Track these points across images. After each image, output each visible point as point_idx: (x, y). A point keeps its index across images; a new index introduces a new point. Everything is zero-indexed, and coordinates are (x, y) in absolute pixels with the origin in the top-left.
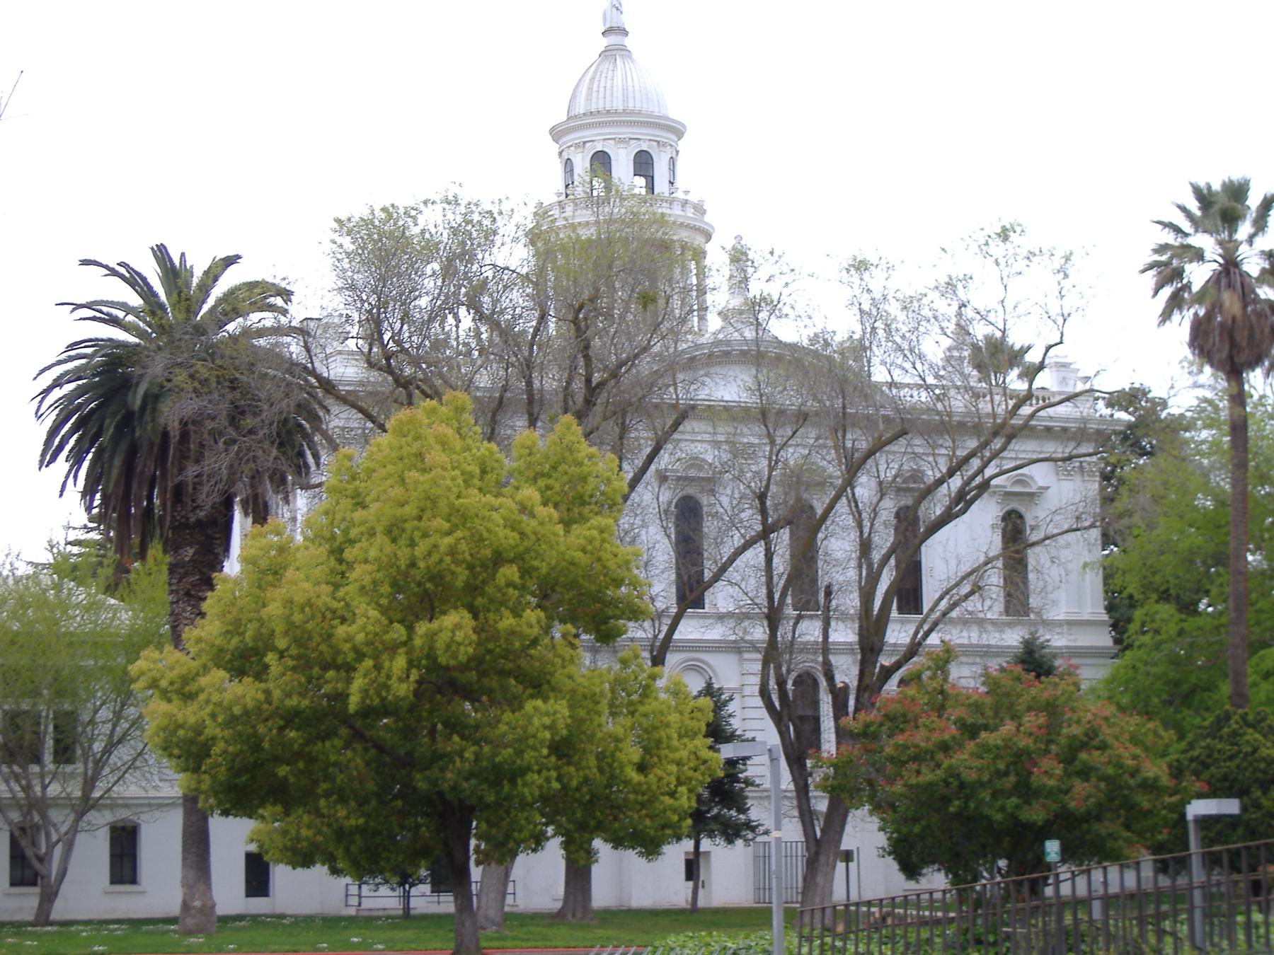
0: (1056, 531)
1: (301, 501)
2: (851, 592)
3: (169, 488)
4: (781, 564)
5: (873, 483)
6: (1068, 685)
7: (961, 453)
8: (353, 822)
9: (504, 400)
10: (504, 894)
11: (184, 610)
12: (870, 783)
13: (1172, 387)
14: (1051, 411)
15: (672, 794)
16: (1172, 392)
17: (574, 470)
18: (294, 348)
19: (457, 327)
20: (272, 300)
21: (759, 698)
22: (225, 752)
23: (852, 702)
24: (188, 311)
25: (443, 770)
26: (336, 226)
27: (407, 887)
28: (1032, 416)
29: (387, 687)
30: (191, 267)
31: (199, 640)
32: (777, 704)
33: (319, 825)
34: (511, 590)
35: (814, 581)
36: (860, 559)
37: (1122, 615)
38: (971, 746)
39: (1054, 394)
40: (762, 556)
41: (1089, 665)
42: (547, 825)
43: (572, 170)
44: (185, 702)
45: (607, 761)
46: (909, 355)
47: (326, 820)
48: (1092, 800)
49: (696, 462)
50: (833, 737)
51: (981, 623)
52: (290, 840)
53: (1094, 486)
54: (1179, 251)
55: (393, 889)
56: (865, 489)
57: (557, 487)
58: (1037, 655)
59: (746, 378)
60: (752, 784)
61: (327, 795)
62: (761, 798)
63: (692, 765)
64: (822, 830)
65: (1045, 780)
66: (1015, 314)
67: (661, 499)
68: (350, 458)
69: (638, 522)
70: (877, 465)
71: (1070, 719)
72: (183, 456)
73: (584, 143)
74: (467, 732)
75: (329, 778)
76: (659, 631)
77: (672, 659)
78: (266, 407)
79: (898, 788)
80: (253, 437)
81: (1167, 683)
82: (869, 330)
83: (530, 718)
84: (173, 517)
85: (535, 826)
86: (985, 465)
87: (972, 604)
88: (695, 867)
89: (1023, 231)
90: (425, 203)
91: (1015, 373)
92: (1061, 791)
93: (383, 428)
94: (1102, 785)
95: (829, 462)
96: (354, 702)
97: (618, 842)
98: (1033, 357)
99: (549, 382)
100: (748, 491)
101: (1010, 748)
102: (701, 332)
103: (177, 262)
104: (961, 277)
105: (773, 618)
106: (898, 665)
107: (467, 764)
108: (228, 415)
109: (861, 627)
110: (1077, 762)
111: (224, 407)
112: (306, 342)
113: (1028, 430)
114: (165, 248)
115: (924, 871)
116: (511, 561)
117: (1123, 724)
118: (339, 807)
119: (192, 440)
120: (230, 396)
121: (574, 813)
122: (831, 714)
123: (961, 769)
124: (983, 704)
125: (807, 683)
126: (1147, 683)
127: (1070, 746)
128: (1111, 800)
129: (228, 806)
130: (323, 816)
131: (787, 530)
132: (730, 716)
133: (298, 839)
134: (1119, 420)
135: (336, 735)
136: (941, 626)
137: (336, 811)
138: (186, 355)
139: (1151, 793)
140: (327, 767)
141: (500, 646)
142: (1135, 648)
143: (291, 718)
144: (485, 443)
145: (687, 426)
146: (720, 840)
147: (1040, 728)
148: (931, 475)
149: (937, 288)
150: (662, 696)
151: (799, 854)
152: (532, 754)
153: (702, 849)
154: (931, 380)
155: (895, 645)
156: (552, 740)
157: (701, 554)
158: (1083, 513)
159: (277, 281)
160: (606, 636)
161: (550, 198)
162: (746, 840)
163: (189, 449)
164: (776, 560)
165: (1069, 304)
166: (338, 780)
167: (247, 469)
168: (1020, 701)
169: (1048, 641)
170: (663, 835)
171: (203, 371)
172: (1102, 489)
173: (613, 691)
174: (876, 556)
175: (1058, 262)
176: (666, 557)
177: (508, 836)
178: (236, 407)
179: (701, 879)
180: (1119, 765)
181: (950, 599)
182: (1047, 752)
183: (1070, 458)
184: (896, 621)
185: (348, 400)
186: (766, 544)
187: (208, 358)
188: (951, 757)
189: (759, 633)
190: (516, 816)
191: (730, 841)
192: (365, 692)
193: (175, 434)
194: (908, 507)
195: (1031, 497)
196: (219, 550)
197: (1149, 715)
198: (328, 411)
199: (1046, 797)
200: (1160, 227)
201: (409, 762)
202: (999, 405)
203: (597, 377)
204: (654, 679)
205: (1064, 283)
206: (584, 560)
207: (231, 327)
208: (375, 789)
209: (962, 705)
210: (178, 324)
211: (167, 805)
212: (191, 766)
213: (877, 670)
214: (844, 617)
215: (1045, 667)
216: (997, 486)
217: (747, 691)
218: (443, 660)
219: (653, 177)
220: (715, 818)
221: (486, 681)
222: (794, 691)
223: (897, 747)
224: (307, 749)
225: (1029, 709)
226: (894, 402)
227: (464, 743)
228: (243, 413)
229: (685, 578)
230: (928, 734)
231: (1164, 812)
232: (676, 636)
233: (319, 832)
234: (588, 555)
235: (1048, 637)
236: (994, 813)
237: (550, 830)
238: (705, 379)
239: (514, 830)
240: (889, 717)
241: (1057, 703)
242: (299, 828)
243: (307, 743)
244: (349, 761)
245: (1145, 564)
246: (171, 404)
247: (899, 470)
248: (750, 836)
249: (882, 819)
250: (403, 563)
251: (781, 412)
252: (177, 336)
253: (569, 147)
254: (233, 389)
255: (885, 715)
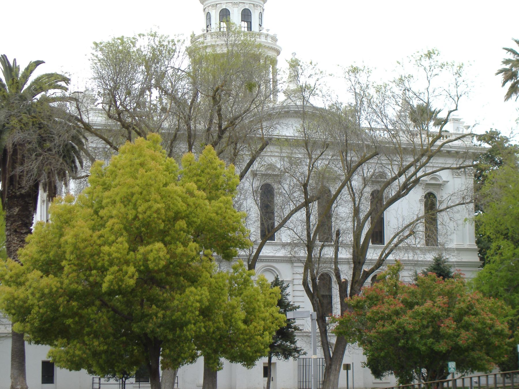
0: (452, 204)
1: (73, 185)
2: (349, 234)
3: (7, 178)
4: (314, 220)
5: (360, 179)
6: (430, 276)
7: (406, 164)
8: (102, 348)
9: (177, 136)
10: (173, 384)
11: (13, 239)
12: (359, 331)
13: (512, 133)
14: (450, 144)
15: (261, 335)
16: (512, 135)
17: (213, 172)
18: (71, 108)
19: (151, 96)
20: (59, 83)
21: (303, 286)
22: (39, 312)
23: (349, 289)
24: (17, 88)
25: (147, 322)
26: (94, 46)
27: (124, 379)
28: (442, 146)
29: (122, 281)
30: (19, 66)
31: (26, 255)
32: (311, 289)
33: (84, 349)
34: (182, 232)
35: (330, 228)
36: (354, 217)
37: (484, 245)
38: (410, 313)
39: (451, 134)
40: (304, 216)
41: (468, 271)
42: (197, 350)
43: (210, 18)
44: (18, 287)
45: (228, 318)
46: (380, 115)
47: (88, 347)
48: (470, 340)
49: (271, 167)
50: (339, 306)
51: (414, 249)
52: (70, 356)
53: (470, 181)
54: (516, 63)
55: (117, 380)
56: (356, 182)
57: (204, 180)
58: (442, 266)
59: (298, 126)
60: (298, 329)
61: (88, 334)
62: (303, 336)
63: (270, 320)
64: (333, 353)
65: (447, 330)
66: (434, 95)
67: (254, 186)
68: (101, 165)
69: (242, 197)
70: (363, 170)
71: (460, 300)
72: (14, 162)
73: (216, 4)
74: (159, 304)
75: (91, 326)
76: (252, 252)
77: (259, 266)
78: (57, 137)
79: (373, 333)
80: (50, 152)
81: (507, 280)
82: (359, 102)
83: (188, 297)
84: (8, 192)
85: (192, 351)
86: (417, 171)
87: (410, 241)
88: (269, 370)
89: (438, 53)
90: (140, 35)
91: (432, 123)
92: (455, 336)
93: (117, 149)
94: (476, 333)
95: (339, 169)
96: (105, 287)
97: (233, 359)
98: (442, 115)
99: (201, 126)
100: (298, 182)
101: (429, 314)
102: (275, 101)
103: (11, 64)
104: (407, 76)
105: (310, 246)
106: (372, 271)
107: (159, 320)
108: (38, 141)
109: (354, 251)
110: (463, 321)
111: (34, 138)
112: (77, 105)
113: (439, 152)
114: (6, 56)
115: (384, 374)
116: (182, 218)
117: (486, 303)
118: (95, 340)
119: (18, 153)
120: (38, 132)
121: (212, 345)
122: (339, 295)
123: (405, 324)
124: (416, 292)
125: (326, 278)
126: (497, 280)
127: (460, 313)
128: (480, 340)
129: (39, 339)
130: (86, 345)
131: (317, 202)
132: (287, 295)
133: (74, 356)
134: (485, 148)
135: (93, 304)
136: (394, 251)
137: (93, 343)
138: (16, 111)
139: (500, 337)
140: (89, 321)
141: (177, 261)
142: (491, 263)
143: (72, 295)
144: (168, 158)
145: (268, 148)
146: (281, 357)
147: (444, 304)
148: (390, 175)
149: (395, 81)
150: (256, 286)
151: (321, 364)
152: (191, 314)
153: (272, 362)
154: (390, 127)
155: (371, 260)
156: (201, 307)
157: (273, 213)
158: (466, 195)
159: (63, 74)
160: (228, 257)
161: (198, 32)
162: (294, 357)
163: (17, 158)
164: (312, 217)
165: (460, 90)
166: (95, 328)
167: (46, 168)
168: (435, 291)
169: (447, 259)
170: (256, 356)
171: (25, 118)
172: (475, 182)
173: (230, 283)
174: (362, 216)
175: (455, 69)
176: (256, 215)
177: (179, 356)
178: (42, 137)
179: (272, 376)
180: (484, 323)
181: (399, 238)
182: (448, 316)
183: (460, 168)
184: (371, 248)
185: (96, 133)
186: (307, 209)
187: (27, 112)
188: (400, 318)
189: (303, 253)
190: (183, 346)
191: (286, 358)
192: (111, 282)
193: (10, 150)
194: (378, 191)
195: (440, 186)
196: (31, 209)
197: (497, 296)
198: (87, 140)
199: (447, 339)
200: (506, 51)
201: (130, 318)
202: (424, 141)
203: (225, 124)
204: (250, 276)
205: (458, 79)
206: (218, 218)
207: (38, 96)
208: (113, 332)
209: (406, 292)
210: (12, 95)
211: (3, 337)
212: (20, 319)
213: (362, 273)
214: (346, 246)
215: (446, 272)
216: (423, 181)
217: (296, 282)
218: (151, 266)
219: (251, 22)
220: (279, 346)
221: (169, 279)
222: (319, 282)
223: (373, 312)
224: (80, 311)
225: (439, 294)
226: (373, 140)
227: (158, 309)
228: (45, 140)
229: (266, 226)
230: (388, 306)
231: (506, 347)
232: (261, 254)
233: (85, 353)
234: (219, 216)
235: (447, 257)
236: (421, 346)
237: (199, 352)
238: (277, 125)
239: (182, 353)
240: (369, 298)
241: (453, 292)
242: (75, 350)
243: (80, 308)
244: (100, 317)
245: (496, 221)
246: (8, 135)
247: (374, 172)
248: (297, 355)
249: (365, 349)
250: (130, 217)
251: (315, 143)
252: (12, 101)
253: (208, 6)
254: (40, 128)
255: (367, 297)
